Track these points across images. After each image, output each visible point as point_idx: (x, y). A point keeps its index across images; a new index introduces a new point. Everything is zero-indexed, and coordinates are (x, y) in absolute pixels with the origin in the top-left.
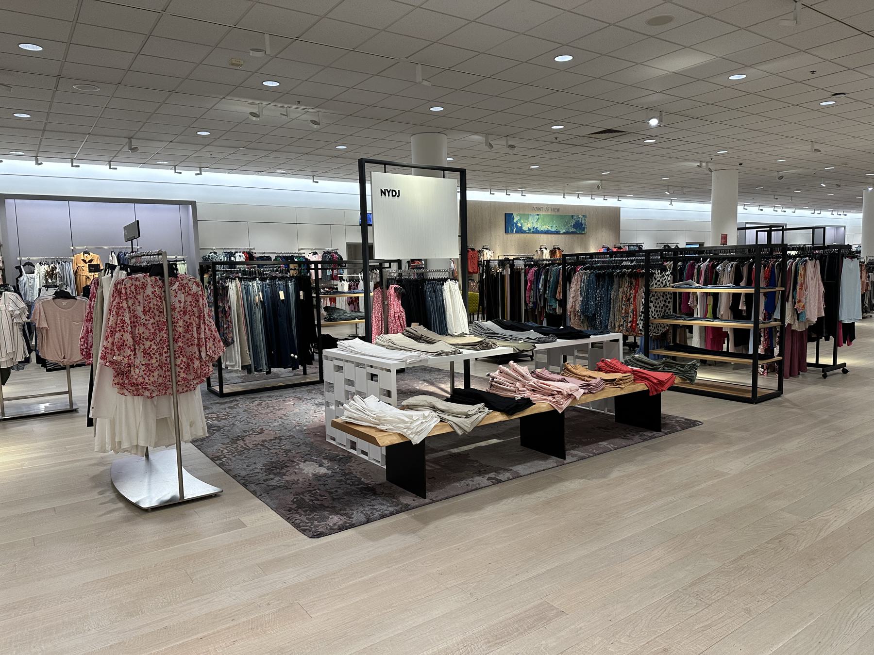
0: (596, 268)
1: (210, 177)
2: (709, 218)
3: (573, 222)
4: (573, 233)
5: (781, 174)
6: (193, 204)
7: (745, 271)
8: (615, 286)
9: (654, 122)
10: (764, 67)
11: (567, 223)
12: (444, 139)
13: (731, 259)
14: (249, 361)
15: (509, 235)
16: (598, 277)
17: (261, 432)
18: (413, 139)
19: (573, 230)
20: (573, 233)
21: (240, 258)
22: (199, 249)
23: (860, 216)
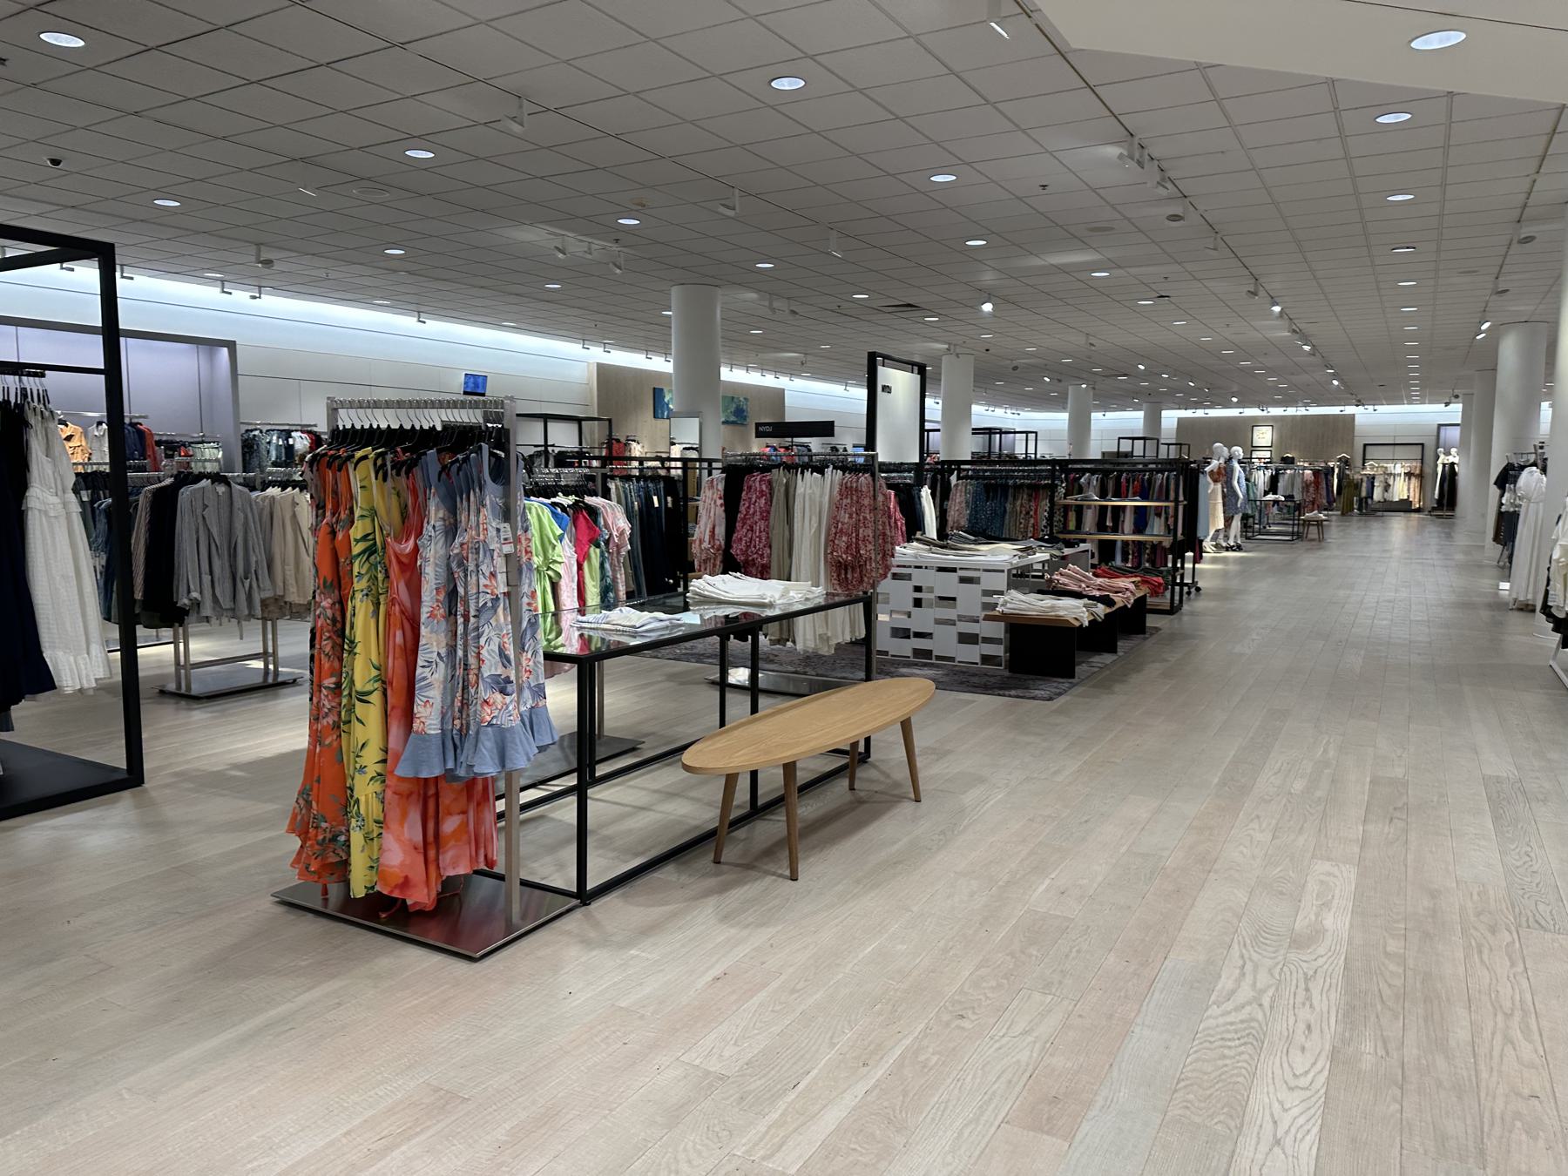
0: (985, 478)
1: (275, 304)
2: (1066, 426)
3: (733, 407)
4: (733, 423)
5: (1015, 363)
6: (231, 346)
7: (1111, 484)
8: (1010, 498)
9: (988, 307)
10: (1133, 271)
11: (725, 410)
12: (719, 291)
13: (1093, 472)
14: (633, 587)
15: (659, 422)
16: (988, 488)
17: (671, 677)
18: (675, 292)
19: (733, 418)
20: (733, 423)
21: (301, 442)
22: (238, 422)
23: (1065, 416)
